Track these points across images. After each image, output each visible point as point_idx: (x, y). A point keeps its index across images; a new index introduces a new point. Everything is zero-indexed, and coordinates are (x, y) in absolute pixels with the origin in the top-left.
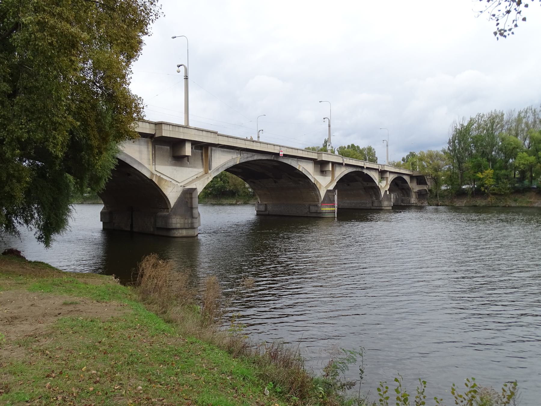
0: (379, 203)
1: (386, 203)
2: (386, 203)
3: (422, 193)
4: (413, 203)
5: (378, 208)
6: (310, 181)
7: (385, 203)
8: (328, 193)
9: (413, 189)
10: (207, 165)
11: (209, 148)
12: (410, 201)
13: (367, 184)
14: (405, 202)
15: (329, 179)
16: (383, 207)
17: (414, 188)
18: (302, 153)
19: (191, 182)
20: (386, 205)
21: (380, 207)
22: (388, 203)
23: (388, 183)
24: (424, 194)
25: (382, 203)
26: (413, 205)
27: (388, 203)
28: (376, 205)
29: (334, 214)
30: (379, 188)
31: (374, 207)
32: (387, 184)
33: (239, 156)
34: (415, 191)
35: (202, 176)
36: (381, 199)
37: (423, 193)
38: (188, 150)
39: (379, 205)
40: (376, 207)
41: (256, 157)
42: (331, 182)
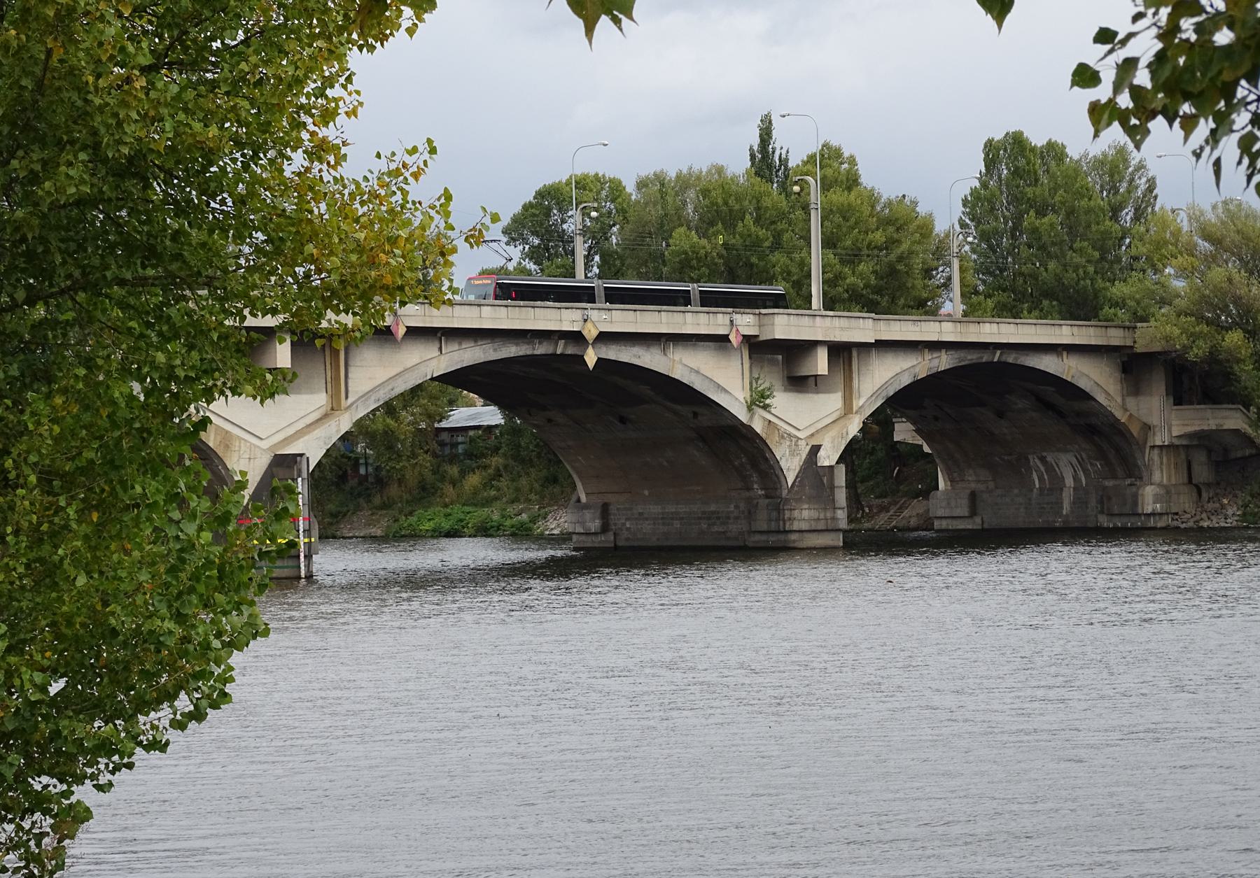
0: (774, 514)
1: (806, 514)
2: (806, 514)
3: (1233, 455)
4: (1153, 514)
5: (772, 539)
6: (726, 414)
7: (804, 515)
8: (274, 469)
9: (1147, 428)
10: (337, 390)
11: (855, 353)
12: (1135, 503)
13: (695, 415)
14: (1116, 510)
15: (831, 403)
16: (793, 537)
17: (1154, 420)
18: (1034, 332)
19: (288, 441)
20: (804, 526)
21: (782, 537)
22: (814, 514)
23: (857, 403)
24: (1244, 458)
25: (787, 514)
26: (1152, 523)
27: (814, 514)
28: (765, 527)
29: (291, 563)
30: (761, 438)
31: (757, 537)
32: (848, 409)
33: (920, 359)
34: (1158, 443)
35: (325, 416)
36: (785, 493)
37: (1239, 454)
38: (821, 363)
39: (773, 526)
40: (764, 538)
41: (511, 350)
42: (325, 416)
